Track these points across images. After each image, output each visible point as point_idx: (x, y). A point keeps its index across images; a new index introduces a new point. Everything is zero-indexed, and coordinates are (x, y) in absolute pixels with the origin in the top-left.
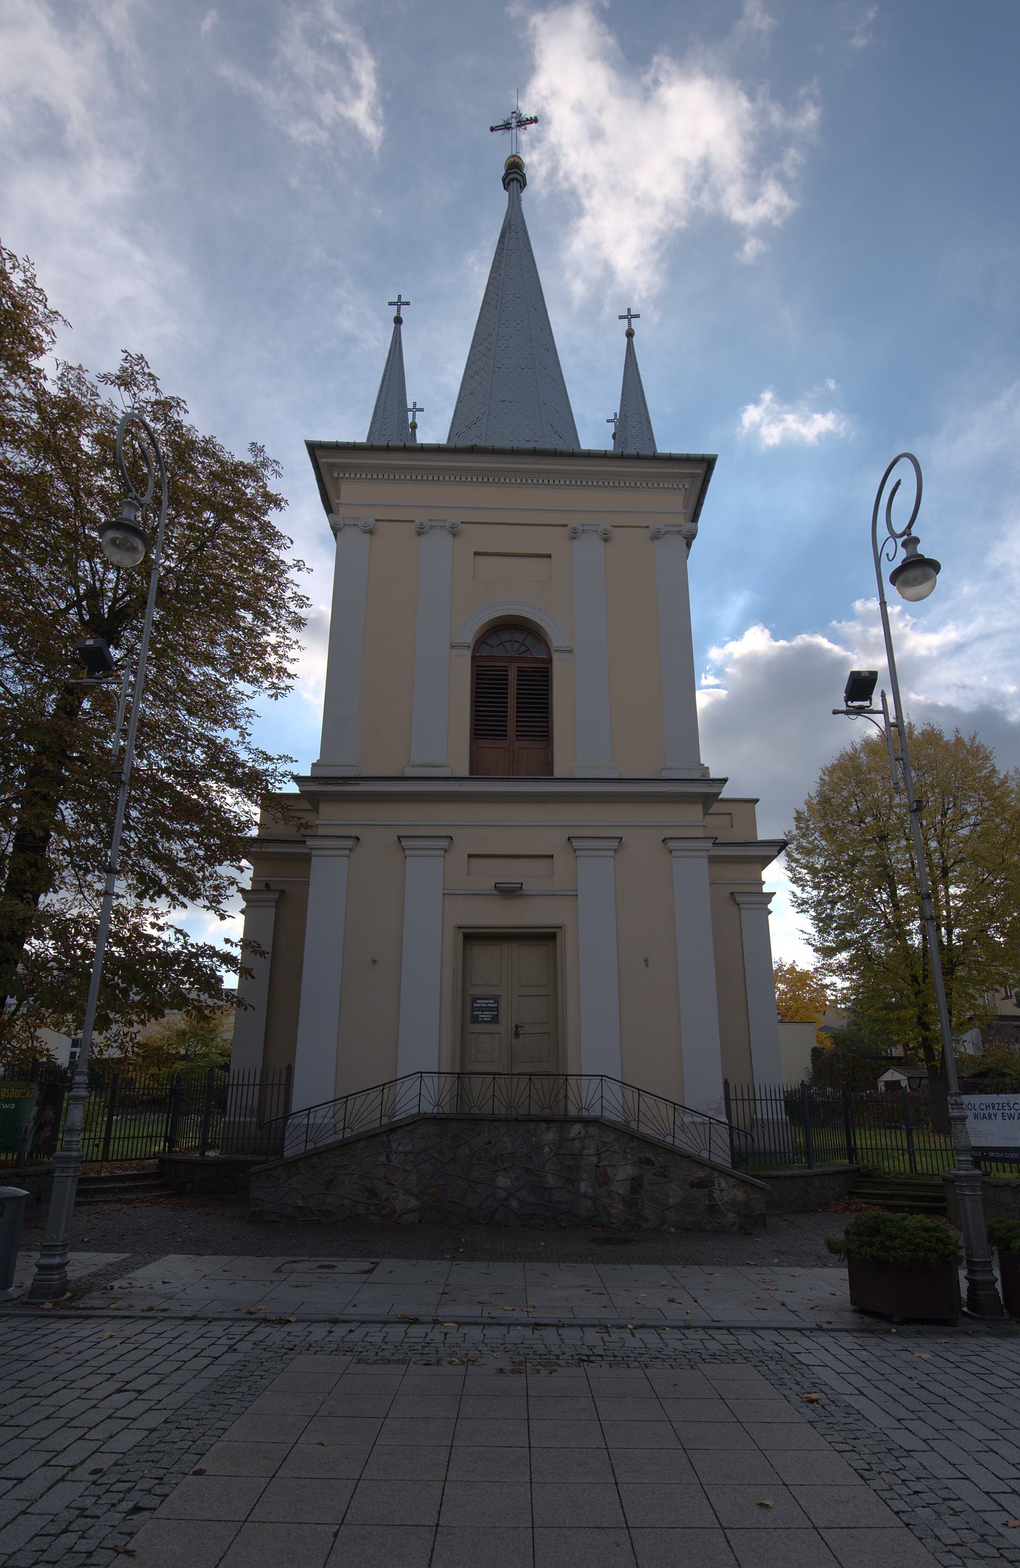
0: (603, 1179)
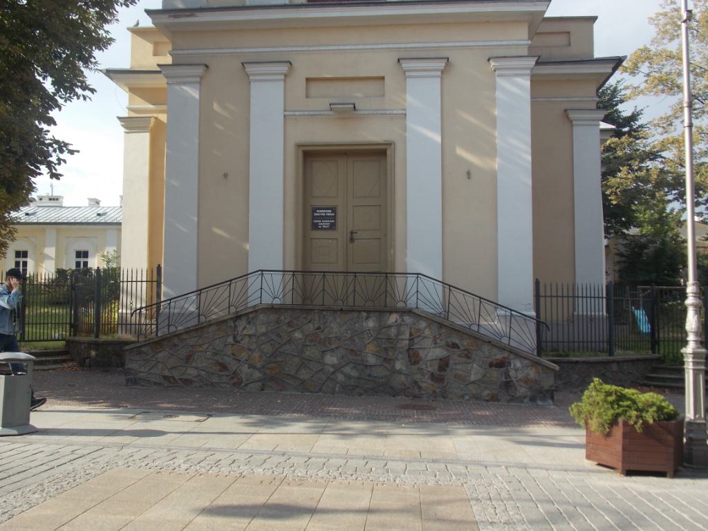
0: (413, 357)
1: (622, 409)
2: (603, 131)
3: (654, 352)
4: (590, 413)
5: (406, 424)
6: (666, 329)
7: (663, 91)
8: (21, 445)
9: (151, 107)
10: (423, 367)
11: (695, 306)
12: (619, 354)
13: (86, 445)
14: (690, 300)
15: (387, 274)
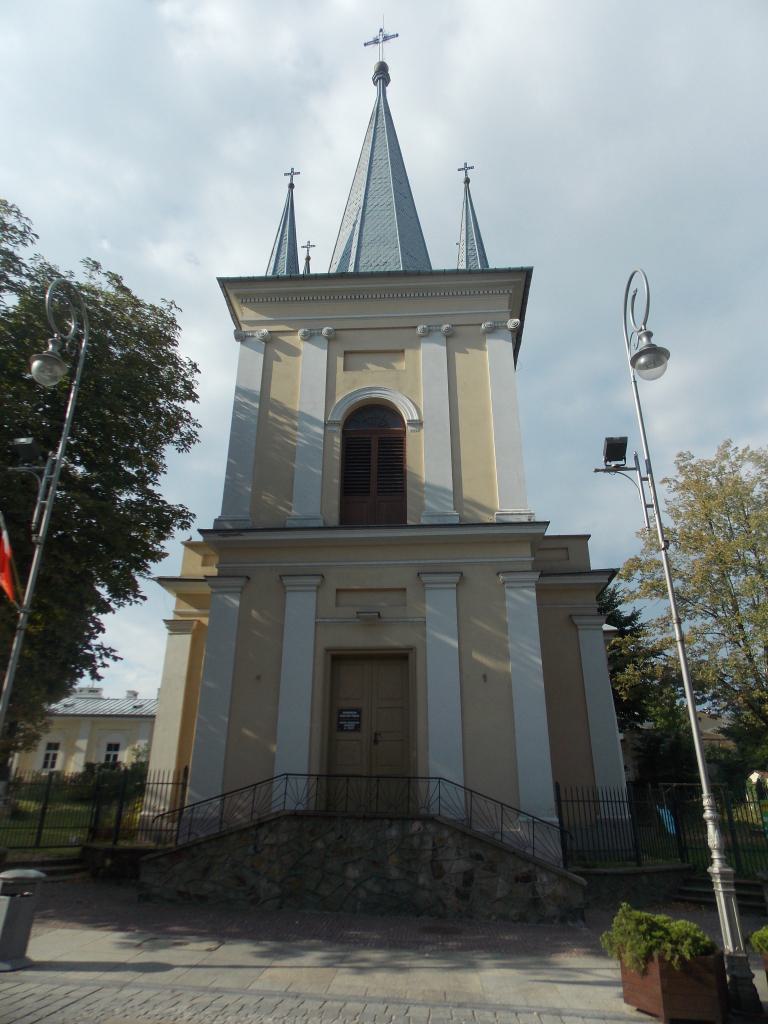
0: (438, 872)
1: (655, 940)
2: (606, 633)
3: (683, 861)
4: (622, 945)
5: (430, 953)
6: (691, 831)
7: (656, 595)
8: (11, 985)
9: (195, 611)
11: (713, 820)
12: (650, 864)
13: (83, 984)
14: (708, 814)
15: (409, 778)
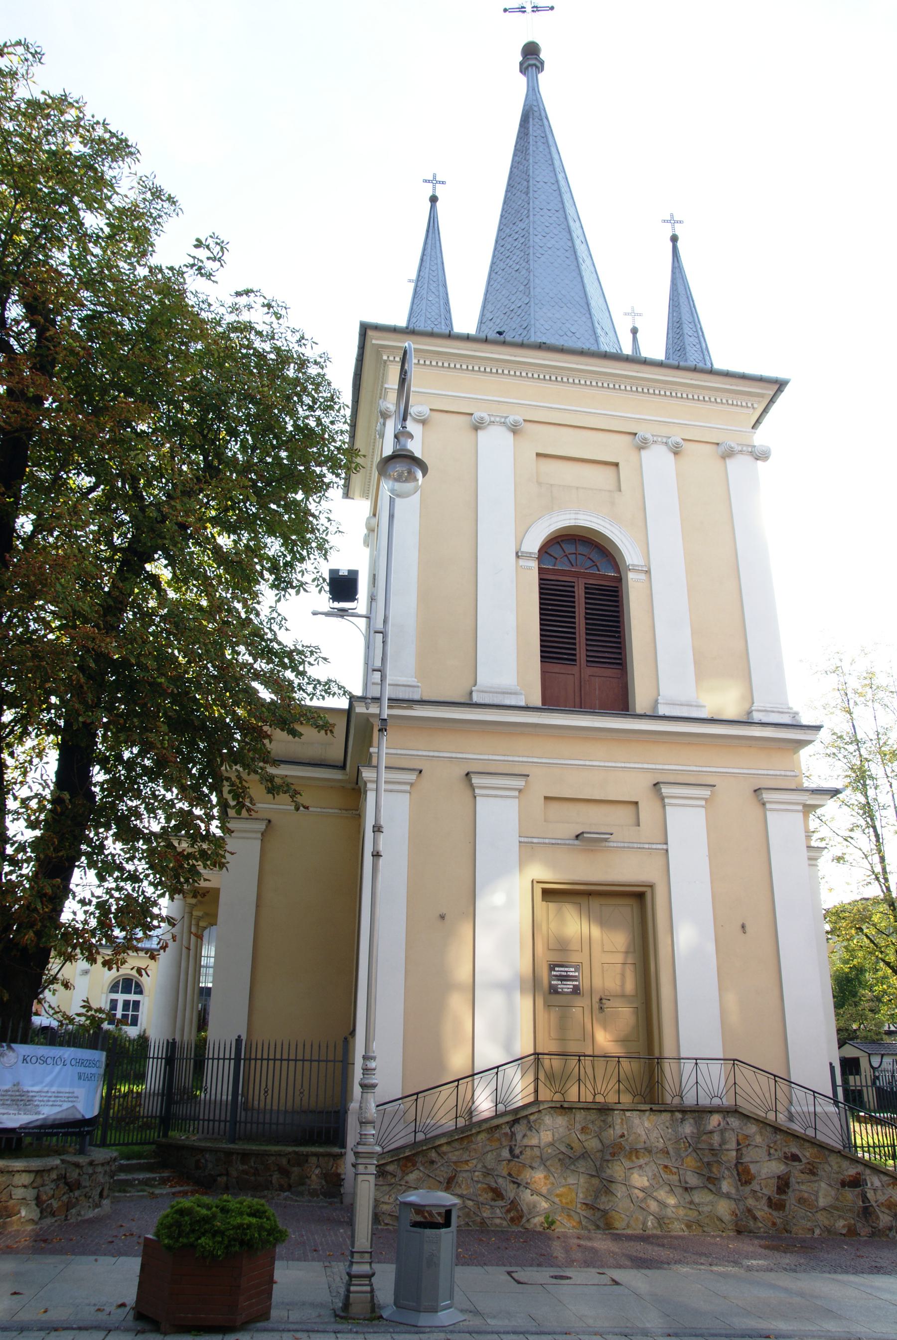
10: (757, 1188)
